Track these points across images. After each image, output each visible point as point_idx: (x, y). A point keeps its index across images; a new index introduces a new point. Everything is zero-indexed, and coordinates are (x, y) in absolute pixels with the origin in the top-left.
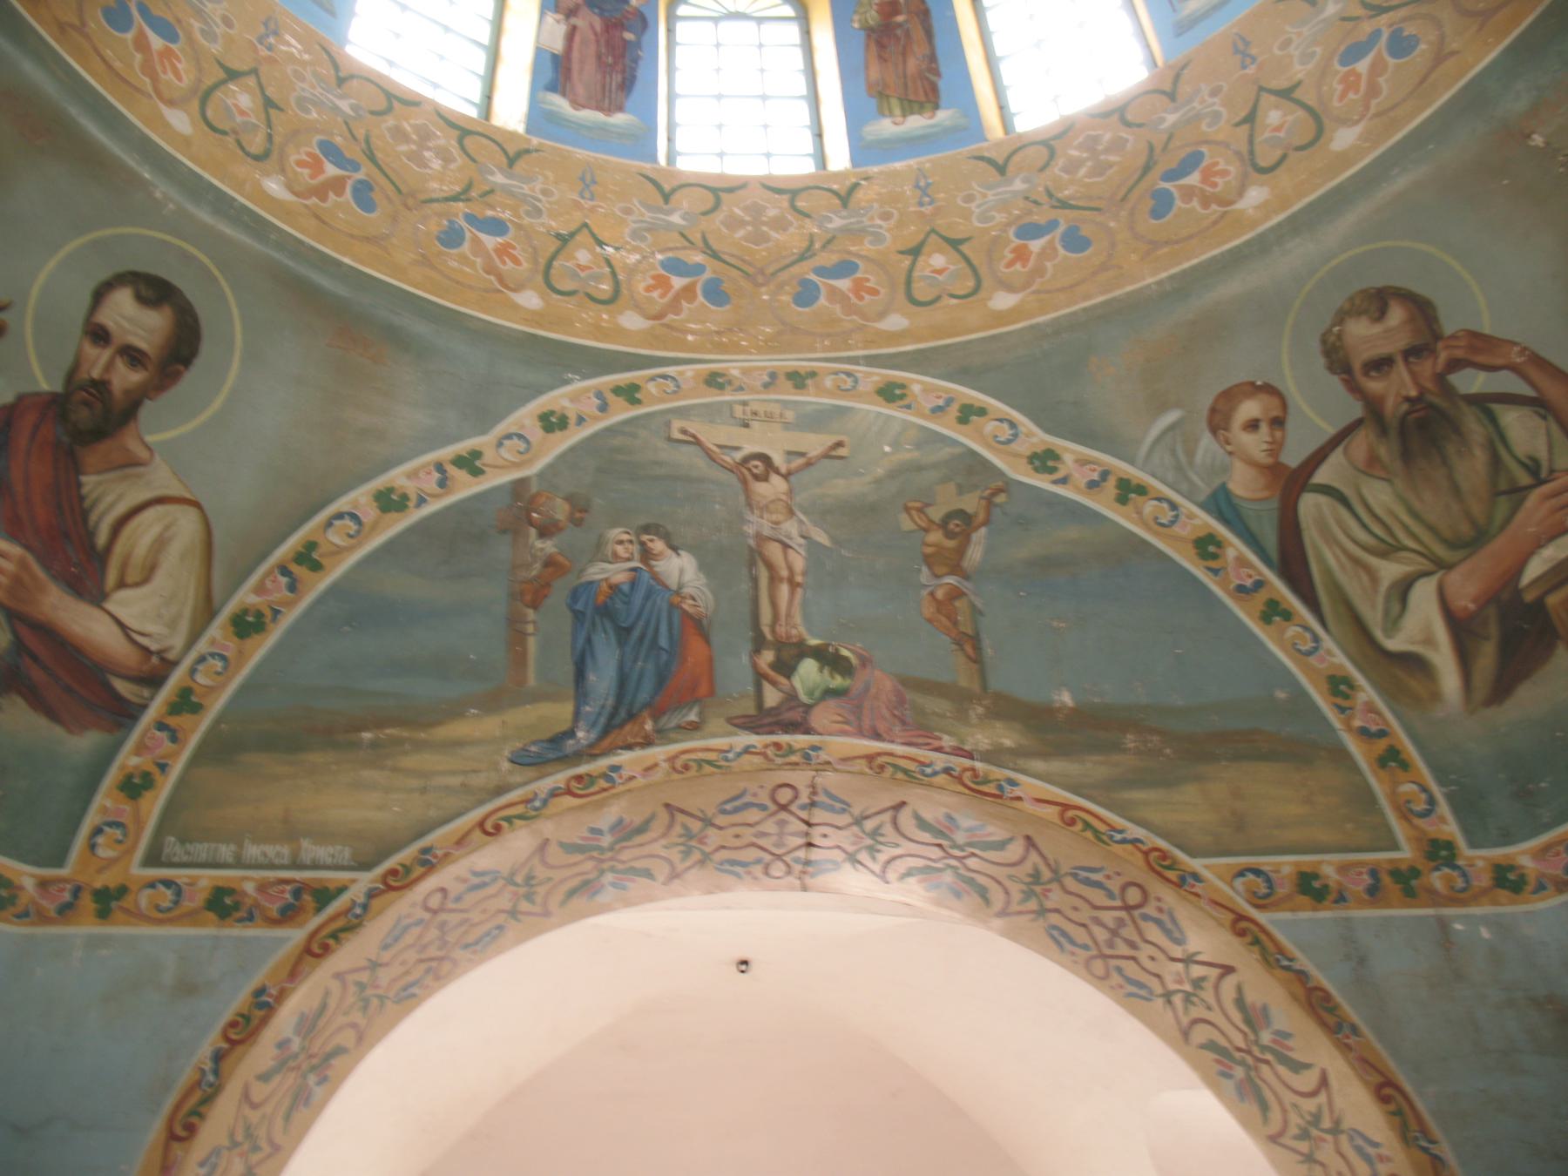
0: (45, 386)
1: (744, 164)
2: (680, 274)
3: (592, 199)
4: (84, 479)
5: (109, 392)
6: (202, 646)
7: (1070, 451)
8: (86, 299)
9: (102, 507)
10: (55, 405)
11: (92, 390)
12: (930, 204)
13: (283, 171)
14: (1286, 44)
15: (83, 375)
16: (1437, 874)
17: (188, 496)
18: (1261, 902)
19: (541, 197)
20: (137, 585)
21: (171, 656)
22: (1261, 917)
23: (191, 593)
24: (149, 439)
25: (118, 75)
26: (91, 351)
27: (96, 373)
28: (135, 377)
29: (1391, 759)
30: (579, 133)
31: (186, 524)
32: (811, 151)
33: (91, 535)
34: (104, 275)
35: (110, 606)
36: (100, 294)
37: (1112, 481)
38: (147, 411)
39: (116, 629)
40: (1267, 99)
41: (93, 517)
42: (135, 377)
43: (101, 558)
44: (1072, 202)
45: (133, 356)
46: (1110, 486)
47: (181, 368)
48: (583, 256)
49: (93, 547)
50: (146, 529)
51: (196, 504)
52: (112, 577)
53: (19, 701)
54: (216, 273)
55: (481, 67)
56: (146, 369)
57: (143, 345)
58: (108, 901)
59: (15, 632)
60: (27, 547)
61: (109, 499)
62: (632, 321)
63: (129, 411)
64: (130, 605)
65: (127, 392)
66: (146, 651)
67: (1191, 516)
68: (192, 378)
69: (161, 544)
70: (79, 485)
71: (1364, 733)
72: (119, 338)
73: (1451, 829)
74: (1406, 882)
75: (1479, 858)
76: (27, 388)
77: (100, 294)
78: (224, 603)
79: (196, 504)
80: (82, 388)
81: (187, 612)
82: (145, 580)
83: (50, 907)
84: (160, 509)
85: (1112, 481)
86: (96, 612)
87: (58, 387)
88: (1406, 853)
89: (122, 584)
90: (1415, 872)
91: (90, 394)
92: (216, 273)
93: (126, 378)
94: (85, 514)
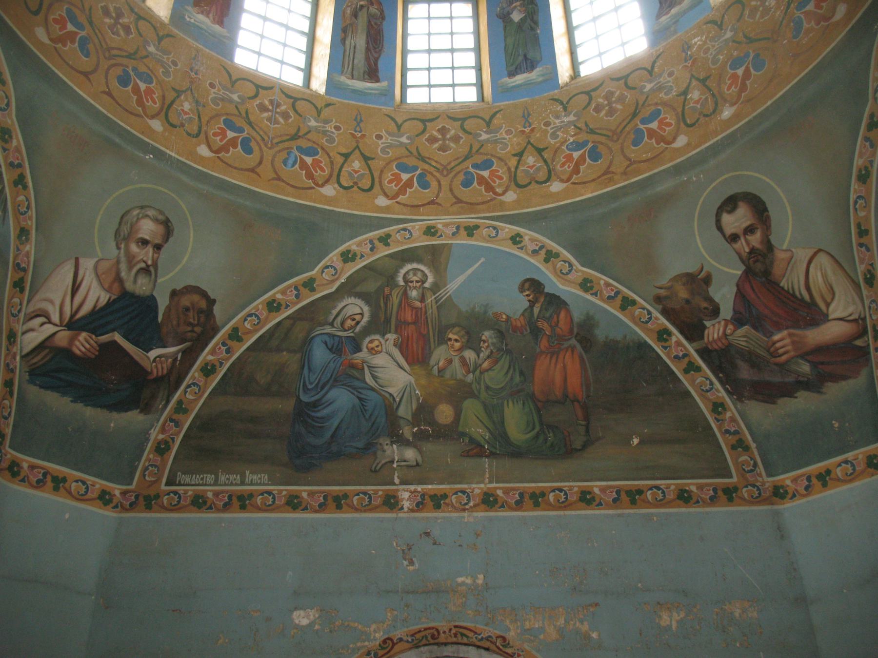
0: (740, 273)
4: (781, 285)
5: (757, 249)
6: (867, 302)
8: (717, 233)
9: (796, 287)
10: (749, 273)
11: (753, 256)
13: (725, 101)
15: (744, 255)
17: (815, 250)
20: (833, 299)
21: (862, 316)
23: (848, 284)
24: (784, 247)
25: (654, 158)
26: (737, 246)
27: (747, 250)
28: (758, 235)
31: (823, 260)
32: (471, 14)
33: (802, 300)
34: (713, 219)
35: (830, 317)
36: (720, 228)
38: (773, 239)
39: (841, 322)
41: (797, 294)
42: (758, 235)
43: (812, 305)
44: (255, 127)
45: (749, 230)
47: (766, 214)
49: (805, 302)
50: (816, 277)
51: (820, 250)
52: (822, 306)
53: (829, 384)
54: (737, 173)
56: (757, 228)
57: (748, 223)
59: (809, 361)
60: (787, 328)
61: (796, 281)
63: (769, 247)
64: (837, 309)
65: (762, 242)
66: (855, 321)
68: (773, 212)
69: (825, 276)
70: (783, 288)
71: (177, 424)
72: (739, 232)
76: (736, 280)
77: (720, 228)
78: (858, 279)
79: (820, 250)
80: (749, 259)
81: (854, 294)
82: (834, 294)
84: (812, 265)
86: (829, 324)
87: (744, 268)
89: (828, 305)
90: (736, 489)
91: (754, 257)
92: (737, 173)
93: (755, 239)
94: (794, 295)
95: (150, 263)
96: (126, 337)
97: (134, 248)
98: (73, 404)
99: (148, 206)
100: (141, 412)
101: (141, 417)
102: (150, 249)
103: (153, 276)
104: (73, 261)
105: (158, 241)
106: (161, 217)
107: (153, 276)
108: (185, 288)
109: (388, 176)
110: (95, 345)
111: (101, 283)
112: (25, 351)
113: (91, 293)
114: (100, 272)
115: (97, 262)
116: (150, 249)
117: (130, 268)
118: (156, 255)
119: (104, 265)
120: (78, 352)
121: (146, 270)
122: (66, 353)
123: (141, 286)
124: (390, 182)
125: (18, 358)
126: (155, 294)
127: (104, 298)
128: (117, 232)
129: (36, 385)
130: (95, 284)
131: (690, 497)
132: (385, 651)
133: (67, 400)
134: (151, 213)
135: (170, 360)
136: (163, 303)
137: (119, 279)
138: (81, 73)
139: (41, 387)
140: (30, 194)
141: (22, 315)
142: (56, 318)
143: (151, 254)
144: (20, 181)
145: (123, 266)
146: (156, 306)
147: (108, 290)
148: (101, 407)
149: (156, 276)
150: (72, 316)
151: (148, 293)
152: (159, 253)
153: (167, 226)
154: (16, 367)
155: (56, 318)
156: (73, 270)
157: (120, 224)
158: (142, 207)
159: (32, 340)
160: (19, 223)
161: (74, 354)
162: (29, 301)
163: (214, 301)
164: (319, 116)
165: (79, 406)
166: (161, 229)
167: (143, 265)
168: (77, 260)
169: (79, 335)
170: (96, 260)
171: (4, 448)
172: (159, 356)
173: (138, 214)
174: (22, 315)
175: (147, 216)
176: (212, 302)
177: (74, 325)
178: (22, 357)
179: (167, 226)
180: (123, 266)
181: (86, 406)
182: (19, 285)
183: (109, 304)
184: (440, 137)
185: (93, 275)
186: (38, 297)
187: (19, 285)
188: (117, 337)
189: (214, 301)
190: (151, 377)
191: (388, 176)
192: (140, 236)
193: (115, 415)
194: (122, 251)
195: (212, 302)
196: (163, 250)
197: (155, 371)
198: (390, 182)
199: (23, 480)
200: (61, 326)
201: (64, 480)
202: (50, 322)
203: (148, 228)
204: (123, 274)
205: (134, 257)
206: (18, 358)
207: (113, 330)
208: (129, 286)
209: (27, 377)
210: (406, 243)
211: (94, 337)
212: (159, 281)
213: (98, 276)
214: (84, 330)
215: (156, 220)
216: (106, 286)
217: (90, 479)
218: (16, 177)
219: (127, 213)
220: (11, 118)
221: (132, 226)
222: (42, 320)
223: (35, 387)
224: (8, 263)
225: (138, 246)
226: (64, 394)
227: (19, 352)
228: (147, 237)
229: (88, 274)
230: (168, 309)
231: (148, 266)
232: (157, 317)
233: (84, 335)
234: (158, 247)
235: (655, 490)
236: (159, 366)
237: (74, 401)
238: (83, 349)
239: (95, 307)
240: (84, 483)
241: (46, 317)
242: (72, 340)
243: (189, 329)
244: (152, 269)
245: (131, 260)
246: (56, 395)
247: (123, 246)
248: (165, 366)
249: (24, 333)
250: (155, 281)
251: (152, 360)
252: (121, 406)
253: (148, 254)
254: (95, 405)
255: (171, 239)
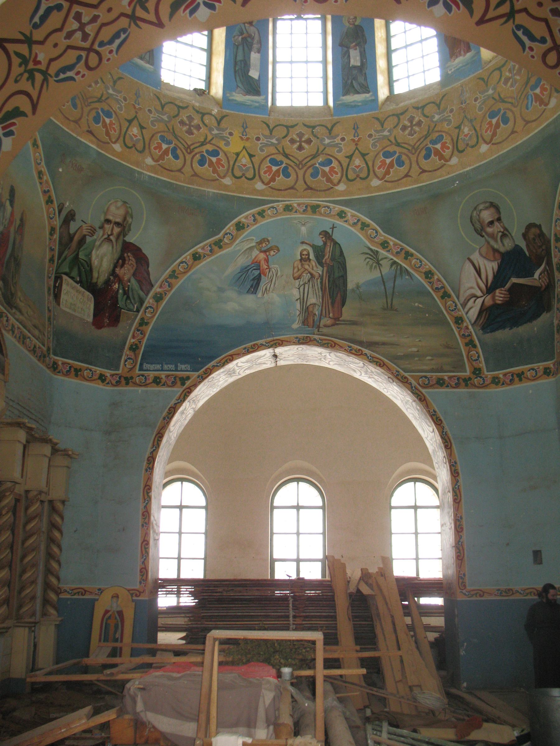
1: (300, 102)
2: (276, 165)
3: (246, 135)
7: (392, 240)
12: (357, 137)
14: (476, 100)
16: (476, 380)
18: (425, 386)
19: (229, 136)
22: (423, 391)
29: (470, 344)
30: (241, 106)
37: (403, 252)
40: (466, 122)
46: (403, 254)
48: (244, 161)
55: (204, 61)
58: (128, 381)
62: (259, 186)
67: (426, 265)
73: (483, 365)
74: (467, 382)
75: (489, 375)
83: (114, 382)
85: (403, 252)
88: (468, 373)
90: (470, 379)
95: (502, 230)
96: (518, 277)
97: (489, 230)
98: (511, 331)
99: (478, 205)
100: (547, 312)
101: (548, 315)
102: (496, 224)
103: (509, 235)
104: (467, 261)
105: (496, 217)
106: (487, 205)
107: (509, 235)
108: (526, 228)
109: (264, 168)
110: (505, 292)
111: (488, 259)
112: (473, 321)
113: (488, 268)
114: (484, 255)
115: (479, 251)
116: (496, 224)
117: (496, 241)
118: (502, 224)
119: (484, 250)
120: (500, 302)
121: (504, 235)
122: (495, 306)
123: (508, 245)
124: (265, 173)
125: (470, 327)
126: (516, 243)
127: (495, 265)
128: (476, 230)
129: (488, 333)
130: (486, 262)
131: (444, 383)
132: (460, 583)
133: (507, 330)
134: (481, 207)
135: (546, 273)
136: (523, 244)
137: (495, 251)
138: (403, 178)
139: (491, 332)
140: (417, 256)
141: (459, 306)
142: (479, 293)
143: (499, 226)
144: (408, 255)
145: (492, 243)
146: (522, 249)
147: (495, 260)
148: (526, 323)
149: (511, 234)
150: (486, 286)
151: (513, 246)
152: (502, 222)
153: (493, 205)
154: (471, 332)
155: (479, 293)
156: (471, 265)
157: (473, 225)
158: (475, 209)
159: (474, 313)
160: (421, 272)
161: (498, 305)
162: (458, 298)
163: (540, 225)
164: (330, 134)
165: (514, 329)
166: (492, 210)
167: (500, 234)
168: (469, 259)
169: (495, 293)
170: (478, 251)
171: (484, 374)
172: (540, 274)
173: (477, 214)
174: (459, 306)
175: (481, 210)
176: (539, 227)
177: (490, 290)
178: (473, 325)
179: (493, 205)
180: (492, 243)
181: (518, 327)
182: (445, 295)
183: (499, 267)
184: (188, 122)
185: (482, 259)
186: (462, 292)
187: (445, 295)
188: (514, 280)
189: (540, 225)
190: (543, 289)
191: (264, 168)
192: (487, 222)
193: (535, 322)
194: (486, 236)
195: (539, 227)
196: (502, 218)
197: (543, 284)
198: (265, 173)
199: (503, 384)
200: (484, 295)
201: (523, 373)
202: (478, 297)
203: (487, 215)
204: (496, 246)
205: (493, 234)
206: (470, 327)
207: (510, 278)
208: (502, 250)
209: (481, 332)
210: (274, 217)
211: (502, 289)
212: (513, 235)
213: (485, 258)
214: (497, 288)
215: (486, 208)
216: (492, 259)
217: (534, 366)
218: (404, 255)
219: (471, 218)
220: (382, 236)
221: (479, 222)
222: (473, 299)
223: (488, 334)
224: (429, 292)
225: (490, 227)
226: (504, 328)
227: (469, 324)
228: (490, 220)
229: (480, 261)
230: (527, 246)
231: (503, 232)
232: (526, 254)
233: (497, 291)
234: (499, 219)
235: (424, 378)
236: (544, 280)
237: (511, 329)
238: (501, 299)
239: (494, 273)
240: (533, 369)
241: (474, 297)
242: (493, 298)
243: (541, 249)
244: (505, 232)
245: (492, 236)
246: (500, 331)
247: (484, 234)
248: (545, 277)
249: (467, 313)
250: (512, 237)
251: (538, 279)
252: (536, 316)
253: (497, 228)
254: (521, 325)
255: (501, 210)
